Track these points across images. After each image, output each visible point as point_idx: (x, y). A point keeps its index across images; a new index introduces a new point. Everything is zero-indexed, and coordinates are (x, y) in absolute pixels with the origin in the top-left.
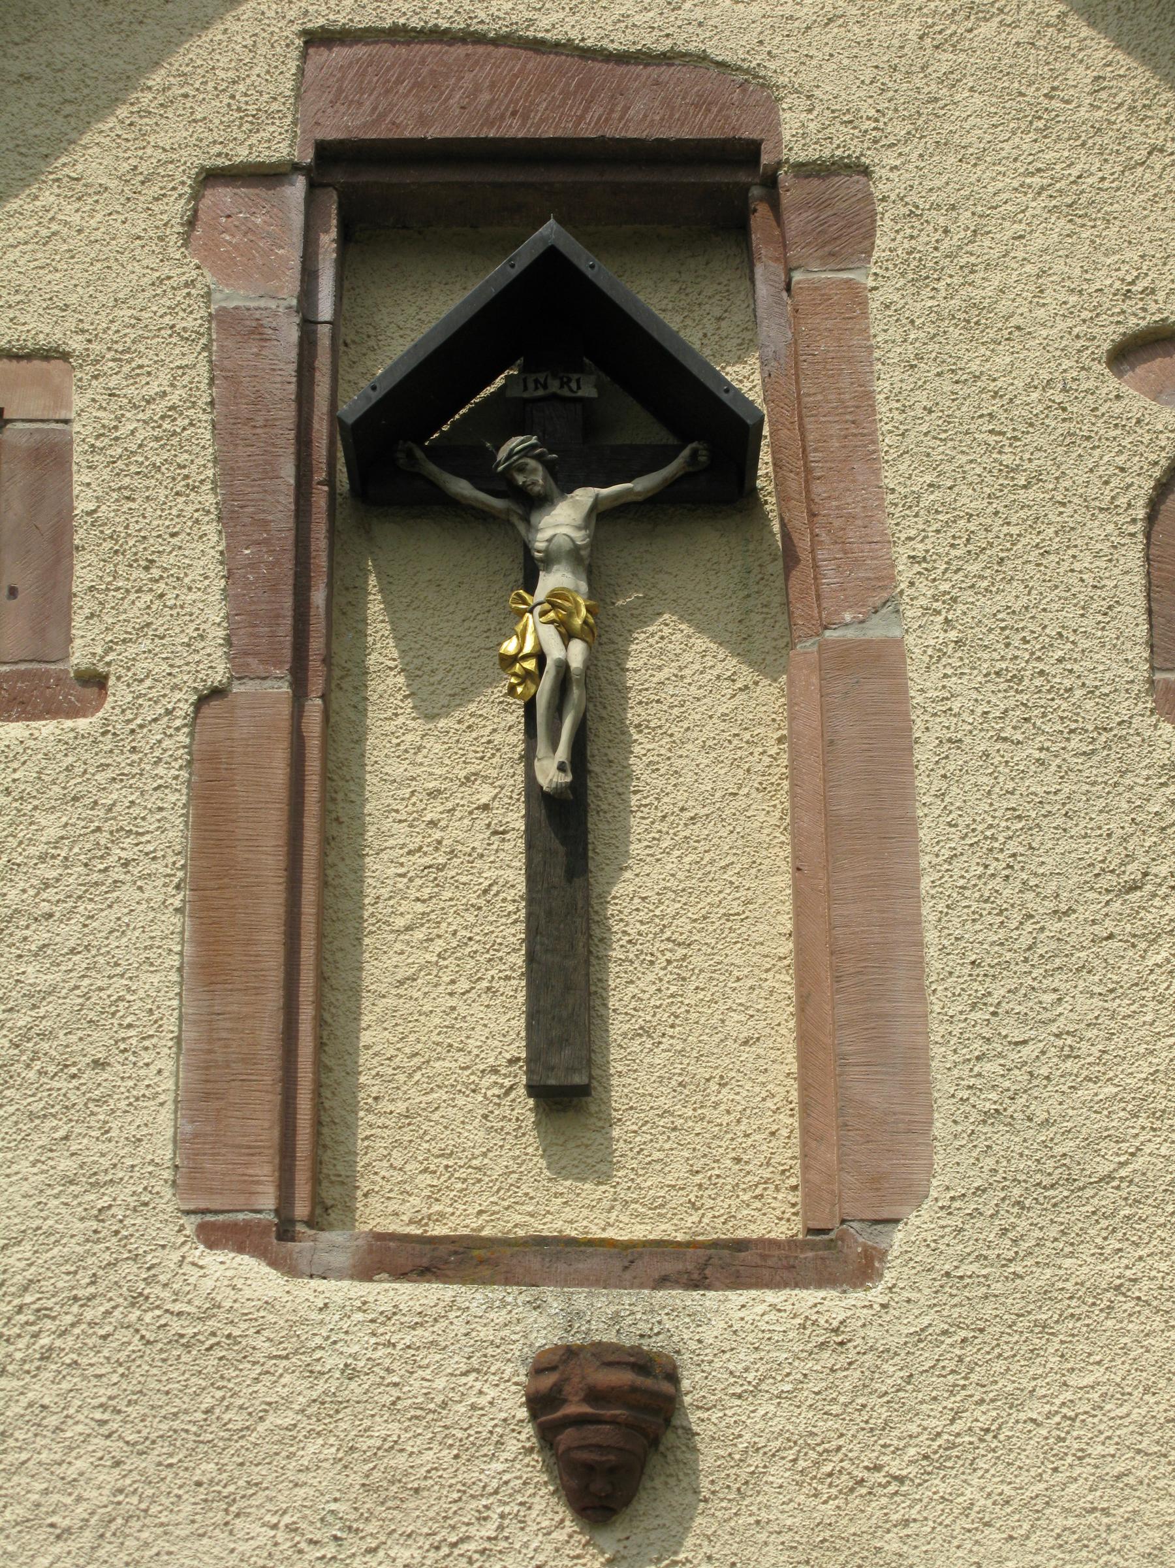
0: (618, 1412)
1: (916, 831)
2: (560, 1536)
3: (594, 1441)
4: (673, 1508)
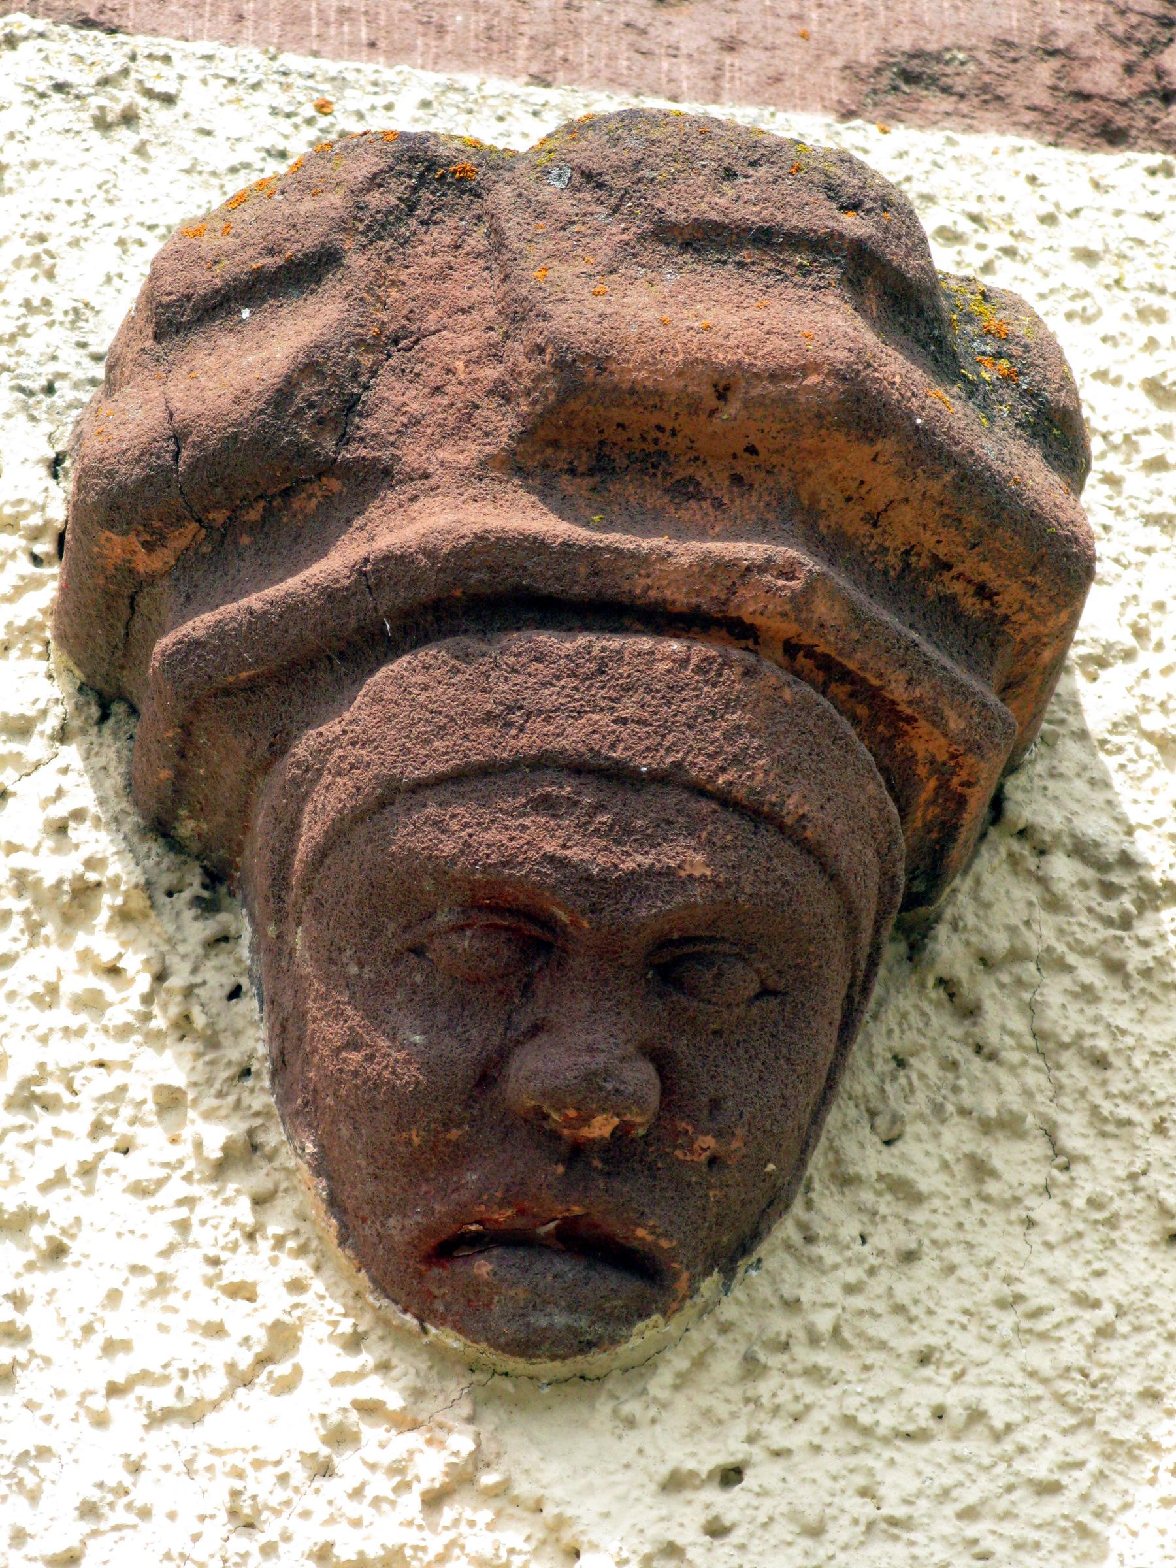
0: (751, 550)
1: (904, 279)
2: (278, 1425)
3: (571, 737)
4: (1033, 1325)
